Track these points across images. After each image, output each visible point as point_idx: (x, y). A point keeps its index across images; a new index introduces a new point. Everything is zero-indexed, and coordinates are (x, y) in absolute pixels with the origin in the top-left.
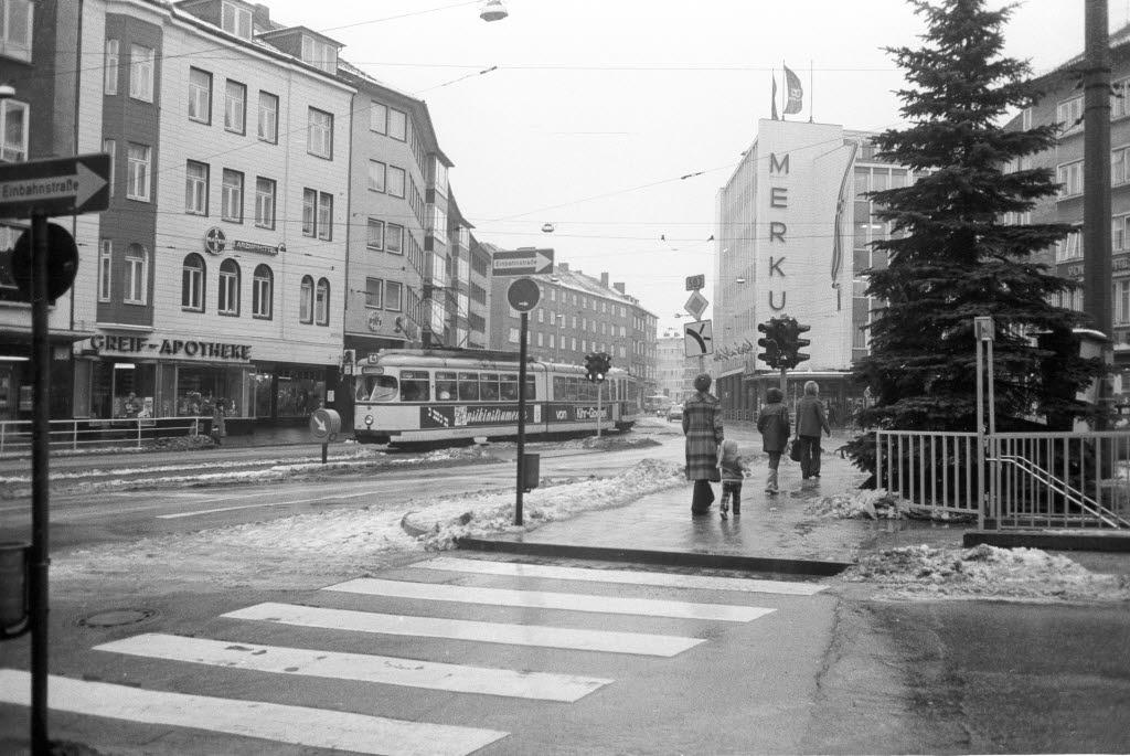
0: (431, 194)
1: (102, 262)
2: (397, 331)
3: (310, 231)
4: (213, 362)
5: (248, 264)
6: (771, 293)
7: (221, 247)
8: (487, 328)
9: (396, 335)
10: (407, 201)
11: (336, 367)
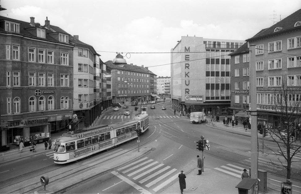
2: (87, 107)
8: (112, 87)
9: (87, 108)
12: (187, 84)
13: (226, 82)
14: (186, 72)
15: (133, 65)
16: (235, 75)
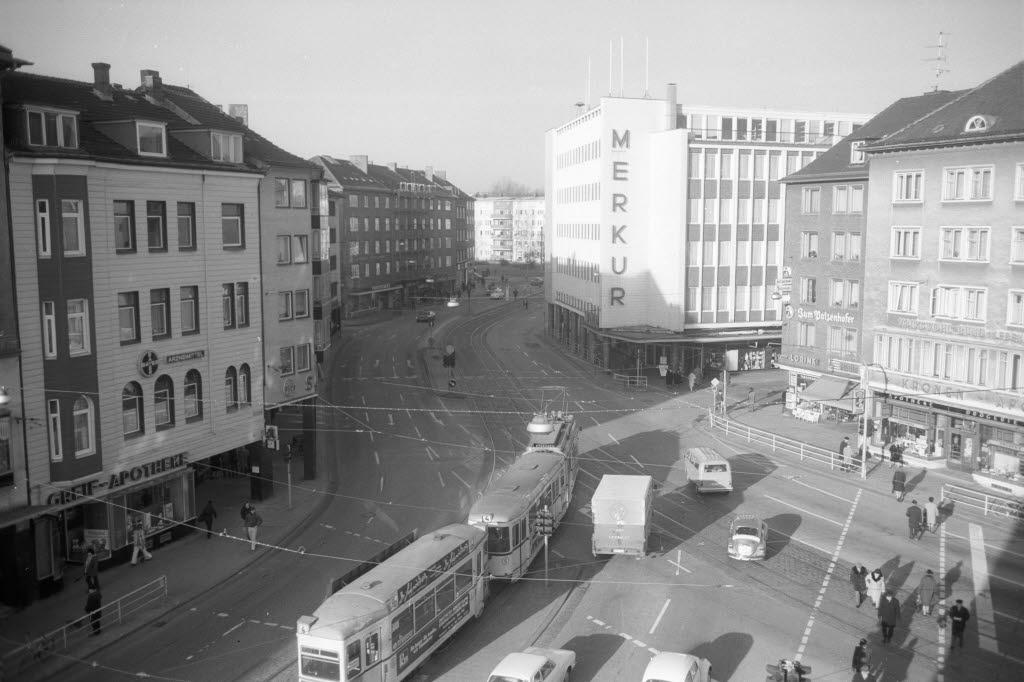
1: (51, 421)
4: (154, 480)
11: (260, 442)
12: (619, 270)
14: (615, 132)
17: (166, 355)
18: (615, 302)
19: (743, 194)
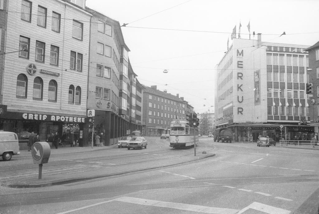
0: (122, 60)
3: (73, 67)
5: (47, 80)
6: (243, 96)
7: (34, 72)
10: (112, 58)
13: (300, 65)
14: (238, 85)
15: (167, 93)
16: (317, 59)
17: (41, 69)
18: (239, 113)
19: (289, 72)
